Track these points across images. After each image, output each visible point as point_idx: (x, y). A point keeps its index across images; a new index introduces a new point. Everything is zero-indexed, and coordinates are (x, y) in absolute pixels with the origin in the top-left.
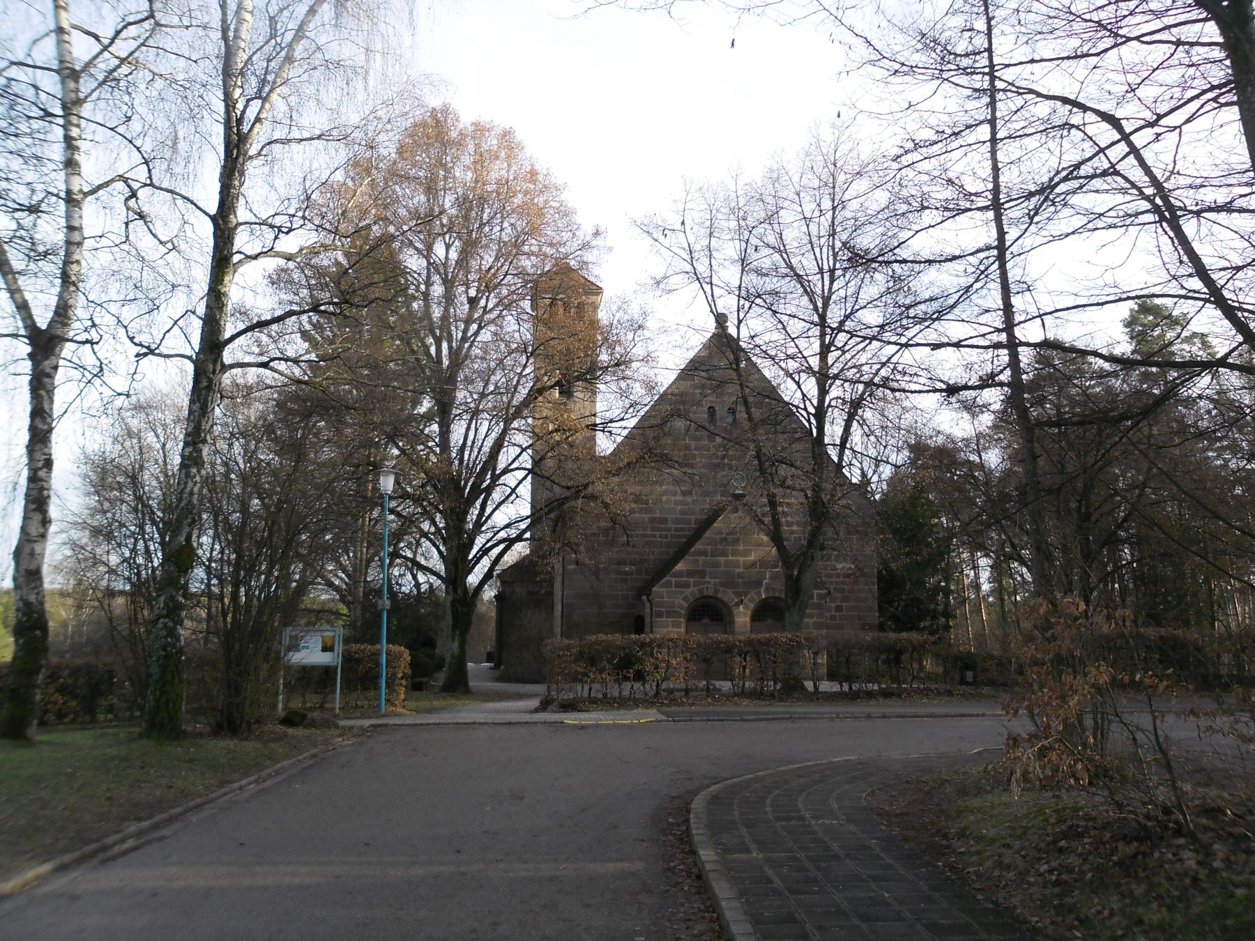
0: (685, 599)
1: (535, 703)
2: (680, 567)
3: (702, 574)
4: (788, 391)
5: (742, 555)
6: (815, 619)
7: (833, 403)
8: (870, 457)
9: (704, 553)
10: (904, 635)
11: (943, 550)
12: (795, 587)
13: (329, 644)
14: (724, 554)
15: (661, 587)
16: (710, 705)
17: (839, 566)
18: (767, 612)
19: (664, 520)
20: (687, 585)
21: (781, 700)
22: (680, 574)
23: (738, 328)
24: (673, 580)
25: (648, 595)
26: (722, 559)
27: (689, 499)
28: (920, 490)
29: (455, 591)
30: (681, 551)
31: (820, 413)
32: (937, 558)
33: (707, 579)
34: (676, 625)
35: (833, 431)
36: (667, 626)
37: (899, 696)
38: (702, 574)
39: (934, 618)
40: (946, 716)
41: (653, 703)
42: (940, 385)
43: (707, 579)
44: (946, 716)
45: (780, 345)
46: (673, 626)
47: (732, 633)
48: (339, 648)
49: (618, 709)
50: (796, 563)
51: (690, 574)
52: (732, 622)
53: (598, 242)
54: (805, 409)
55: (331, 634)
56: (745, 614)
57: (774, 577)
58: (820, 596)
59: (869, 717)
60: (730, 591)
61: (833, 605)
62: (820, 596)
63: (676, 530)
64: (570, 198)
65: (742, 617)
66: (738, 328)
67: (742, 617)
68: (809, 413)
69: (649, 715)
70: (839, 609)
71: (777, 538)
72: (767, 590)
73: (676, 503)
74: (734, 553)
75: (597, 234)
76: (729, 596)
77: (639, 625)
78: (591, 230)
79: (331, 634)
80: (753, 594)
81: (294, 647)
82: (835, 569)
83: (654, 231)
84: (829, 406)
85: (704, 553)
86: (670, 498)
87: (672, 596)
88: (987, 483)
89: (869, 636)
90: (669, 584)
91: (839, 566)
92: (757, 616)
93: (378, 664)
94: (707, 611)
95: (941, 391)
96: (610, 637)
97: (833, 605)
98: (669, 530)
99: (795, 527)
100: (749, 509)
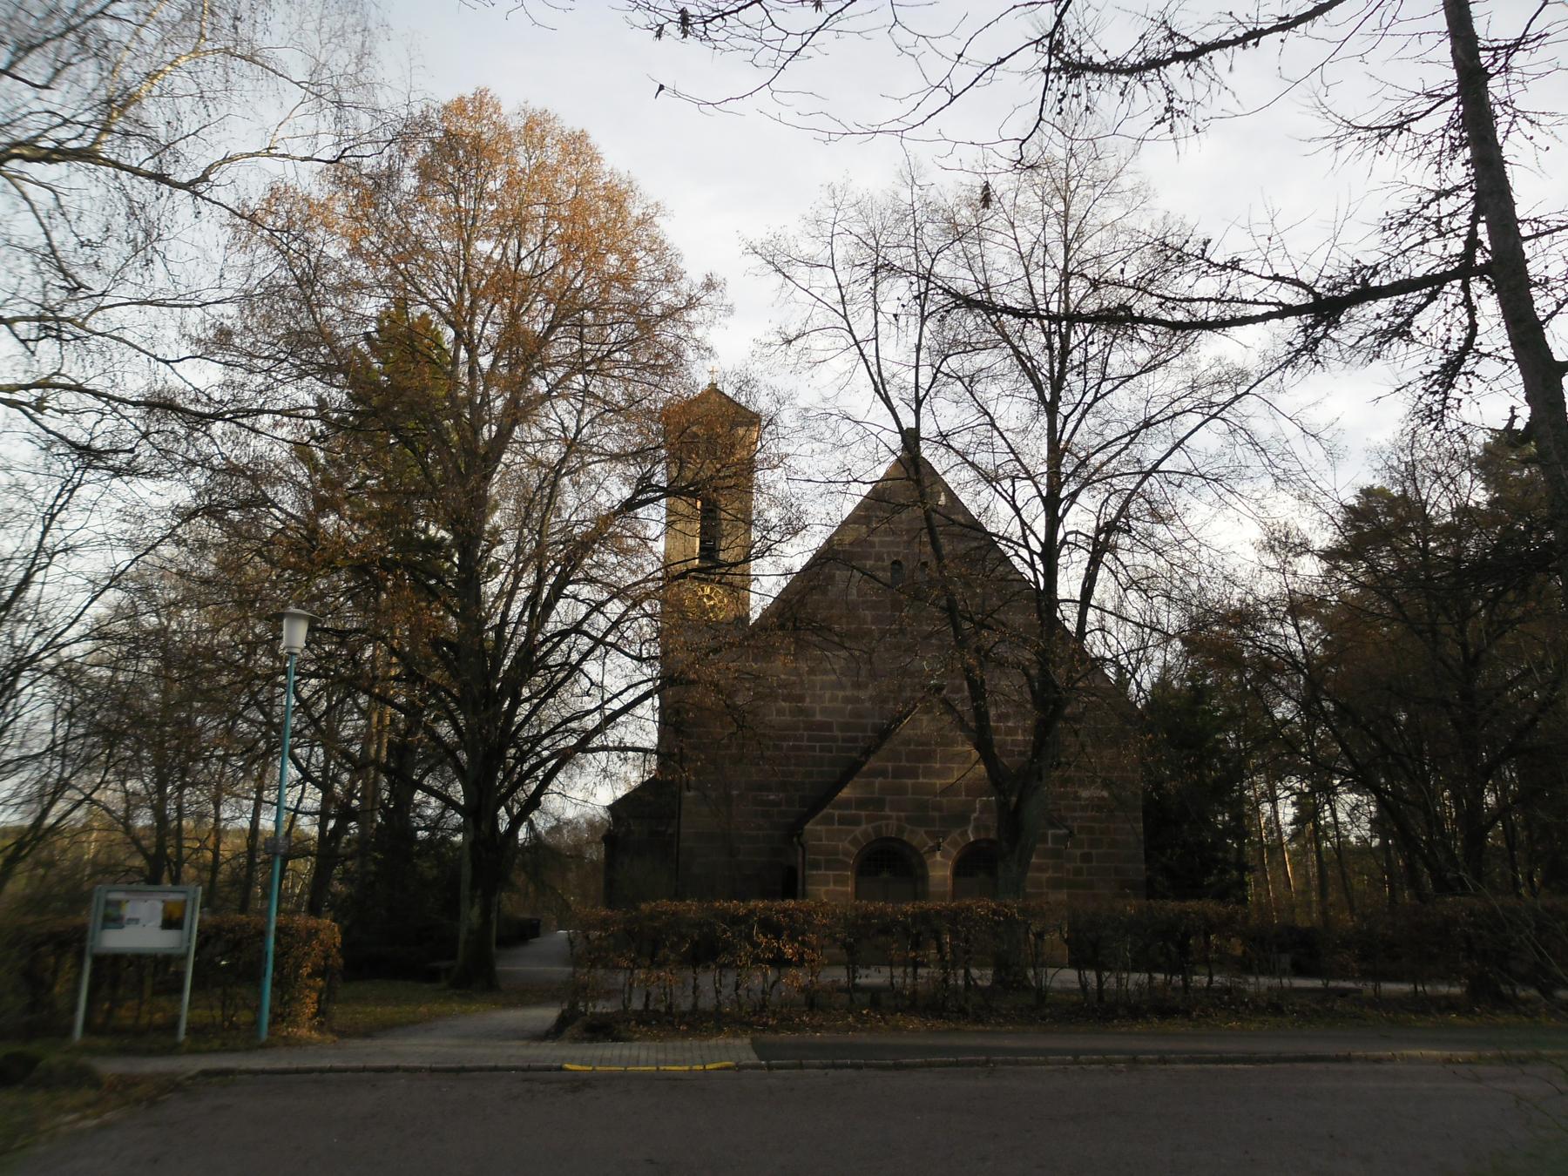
0: (854, 841)
1: (548, 1015)
2: (845, 793)
3: (879, 804)
4: (1000, 520)
5: (938, 777)
6: (1049, 874)
7: (1070, 538)
8: (1123, 628)
9: (882, 773)
10: (1192, 905)
11: (1236, 772)
12: (1012, 822)
13: (177, 915)
14: (913, 774)
15: (818, 823)
16: (851, 1028)
17: (1085, 794)
18: (973, 863)
19: (827, 726)
20: (855, 821)
21: (978, 1020)
22: (846, 804)
23: (917, 413)
24: (837, 813)
25: (799, 836)
26: (909, 782)
27: (863, 695)
28: (1199, 694)
29: (477, 827)
30: (851, 771)
31: (1050, 552)
32: (1225, 787)
33: (888, 812)
34: (839, 881)
35: (1068, 586)
36: (827, 883)
37: (1187, 1014)
38: (879, 804)
39: (1223, 871)
40: (1276, 1059)
41: (750, 1025)
42: (1290, 296)
43: (888, 812)
44: (1276, 1059)
45: (986, 440)
46: (835, 883)
47: (925, 895)
48: (194, 919)
49: (685, 1035)
50: (1012, 786)
51: (861, 804)
52: (924, 878)
53: (712, 297)
54: (1027, 546)
55: (180, 897)
56: (945, 865)
57: (985, 808)
58: (1056, 839)
59: (1134, 1060)
60: (922, 831)
61: (1078, 852)
62: (1056, 839)
63: (844, 740)
64: (670, 230)
65: (940, 870)
66: (917, 413)
67: (940, 870)
68: (1032, 552)
69: (726, 1052)
70: (1086, 858)
71: (983, 741)
72: (977, 829)
73: (847, 700)
74: (929, 773)
75: (710, 285)
76: (918, 837)
77: (790, 885)
78: (700, 280)
79: (180, 897)
80: (955, 834)
81: (114, 920)
82: (1077, 798)
83: (778, 263)
84: (1064, 542)
85: (882, 773)
86: (827, 690)
87: (834, 836)
88: (1307, 665)
89: (1131, 907)
90: (829, 820)
91: (1085, 794)
92: (963, 868)
93: (262, 955)
94: (889, 862)
95: (1286, 311)
96: (680, 906)
97: (1078, 852)
98: (834, 739)
99: (1014, 733)
100: (949, 706)
